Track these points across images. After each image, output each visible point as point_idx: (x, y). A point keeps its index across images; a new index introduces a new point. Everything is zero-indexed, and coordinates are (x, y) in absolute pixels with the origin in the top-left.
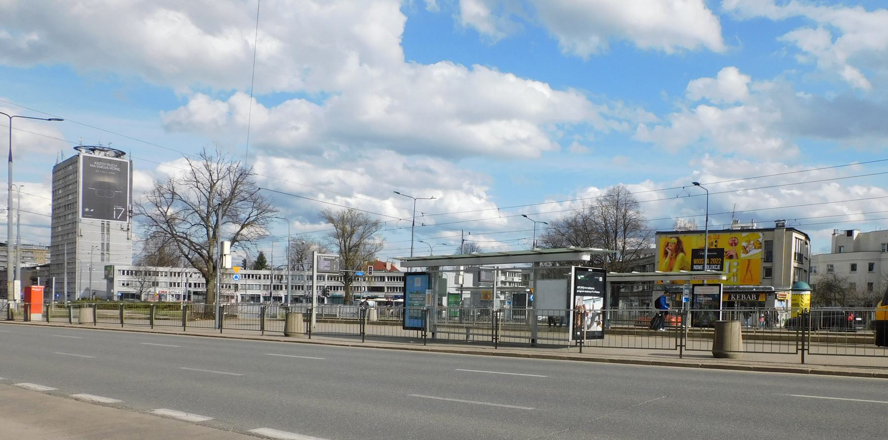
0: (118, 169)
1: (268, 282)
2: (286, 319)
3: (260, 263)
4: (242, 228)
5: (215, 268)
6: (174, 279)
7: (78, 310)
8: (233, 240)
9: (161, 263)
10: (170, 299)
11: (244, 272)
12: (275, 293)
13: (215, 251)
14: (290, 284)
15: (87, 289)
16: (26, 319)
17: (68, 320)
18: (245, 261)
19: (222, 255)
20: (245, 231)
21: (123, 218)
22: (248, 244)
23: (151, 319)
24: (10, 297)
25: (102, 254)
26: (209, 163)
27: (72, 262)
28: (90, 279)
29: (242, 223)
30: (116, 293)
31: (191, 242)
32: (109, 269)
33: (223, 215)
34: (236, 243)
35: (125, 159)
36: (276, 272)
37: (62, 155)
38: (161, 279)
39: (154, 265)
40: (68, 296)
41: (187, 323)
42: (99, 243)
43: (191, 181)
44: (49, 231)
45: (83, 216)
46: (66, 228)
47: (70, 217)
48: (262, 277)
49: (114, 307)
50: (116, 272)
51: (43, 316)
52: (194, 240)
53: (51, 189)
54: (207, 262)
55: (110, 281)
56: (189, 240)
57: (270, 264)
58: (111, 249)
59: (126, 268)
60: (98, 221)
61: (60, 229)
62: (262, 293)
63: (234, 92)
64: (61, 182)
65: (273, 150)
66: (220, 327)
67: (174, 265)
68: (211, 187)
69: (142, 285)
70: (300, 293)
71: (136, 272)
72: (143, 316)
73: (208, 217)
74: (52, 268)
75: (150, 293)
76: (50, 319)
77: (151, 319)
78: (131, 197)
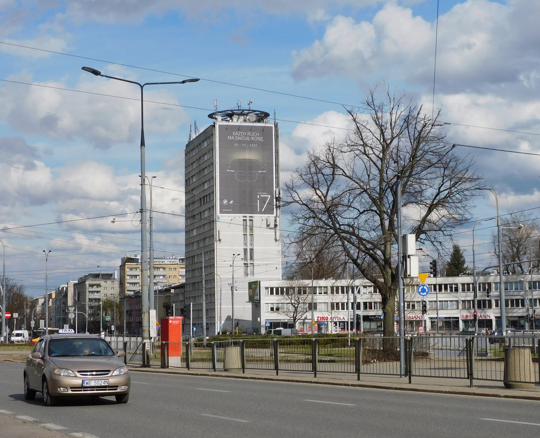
0: (261, 139)
1: (470, 296)
2: (506, 356)
3: (456, 266)
4: (430, 211)
5: (394, 278)
6: (340, 298)
7: (221, 351)
8: (419, 231)
9: (321, 274)
10: (332, 330)
11: (433, 281)
12: (481, 314)
13: (394, 250)
14: (504, 298)
15: (229, 319)
16: (164, 365)
17: (210, 365)
18: (434, 264)
19: (405, 257)
20: (434, 216)
21: (269, 211)
22: (440, 237)
23: (313, 362)
24: (146, 335)
25: (246, 265)
26: (379, 115)
27: (211, 280)
28: (230, 305)
29: (429, 202)
30: (263, 323)
31: (360, 239)
32: (254, 287)
33: (403, 192)
34: (423, 236)
35: (269, 123)
36: (481, 279)
37: (196, 128)
38: (320, 298)
39: (309, 278)
40: (207, 329)
41: (363, 368)
42: (240, 249)
43: (356, 145)
44: (181, 238)
45: (221, 212)
46: (202, 231)
47: (206, 214)
48: (460, 287)
49: (263, 345)
50: (263, 291)
51: (182, 360)
52: (364, 235)
53: (182, 179)
54: (383, 269)
55: (256, 303)
56: (357, 236)
57: (471, 266)
58: (253, 256)
59: (275, 284)
60: (239, 217)
61: (195, 233)
62: (461, 314)
63: (380, 7)
64: (195, 165)
65: (441, 83)
66: (408, 373)
67: (338, 277)
68: (384, 151)
69: (296, 309)
70: (519, 312)
71: (288, 289)
72: (302, 357)
73: (381, 199)
74: (188, 289)
75: (307, 322)
76: (192, 365)
77: (313, 362)
78: (277, 178)
